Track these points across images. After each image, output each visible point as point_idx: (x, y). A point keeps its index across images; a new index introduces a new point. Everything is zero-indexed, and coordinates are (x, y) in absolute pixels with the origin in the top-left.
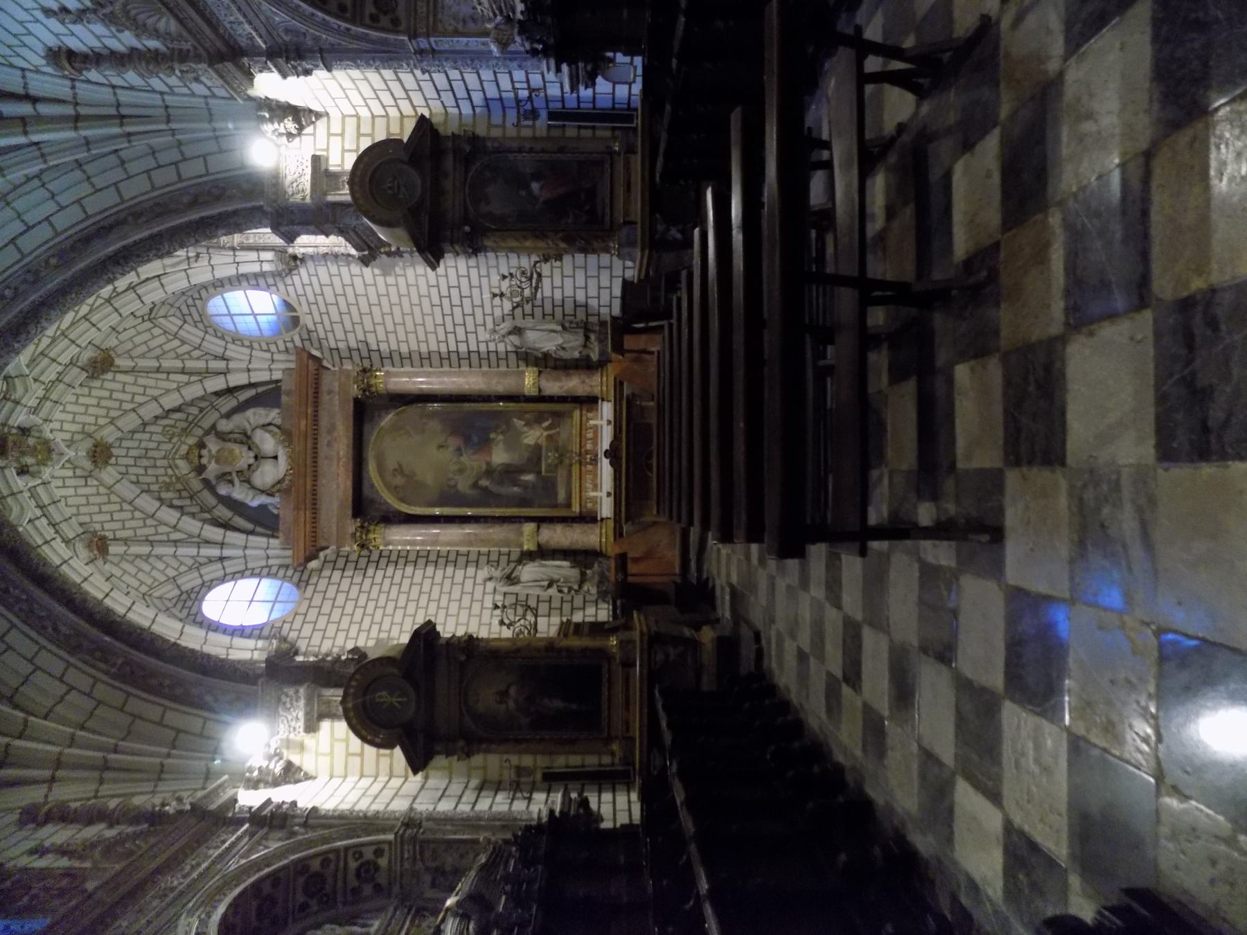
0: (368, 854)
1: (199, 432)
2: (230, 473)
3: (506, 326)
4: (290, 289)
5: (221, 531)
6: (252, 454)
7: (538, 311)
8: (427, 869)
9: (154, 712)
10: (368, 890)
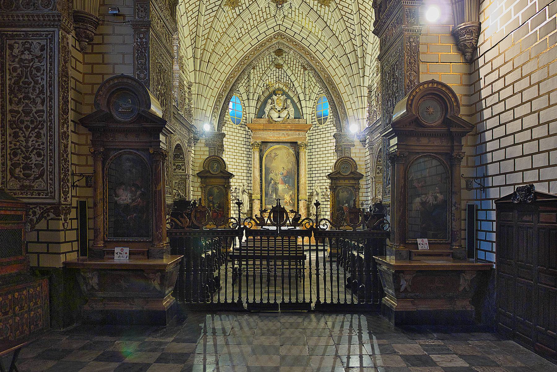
0: (183, 167)
3: (319, 191)
4: (329, 123)
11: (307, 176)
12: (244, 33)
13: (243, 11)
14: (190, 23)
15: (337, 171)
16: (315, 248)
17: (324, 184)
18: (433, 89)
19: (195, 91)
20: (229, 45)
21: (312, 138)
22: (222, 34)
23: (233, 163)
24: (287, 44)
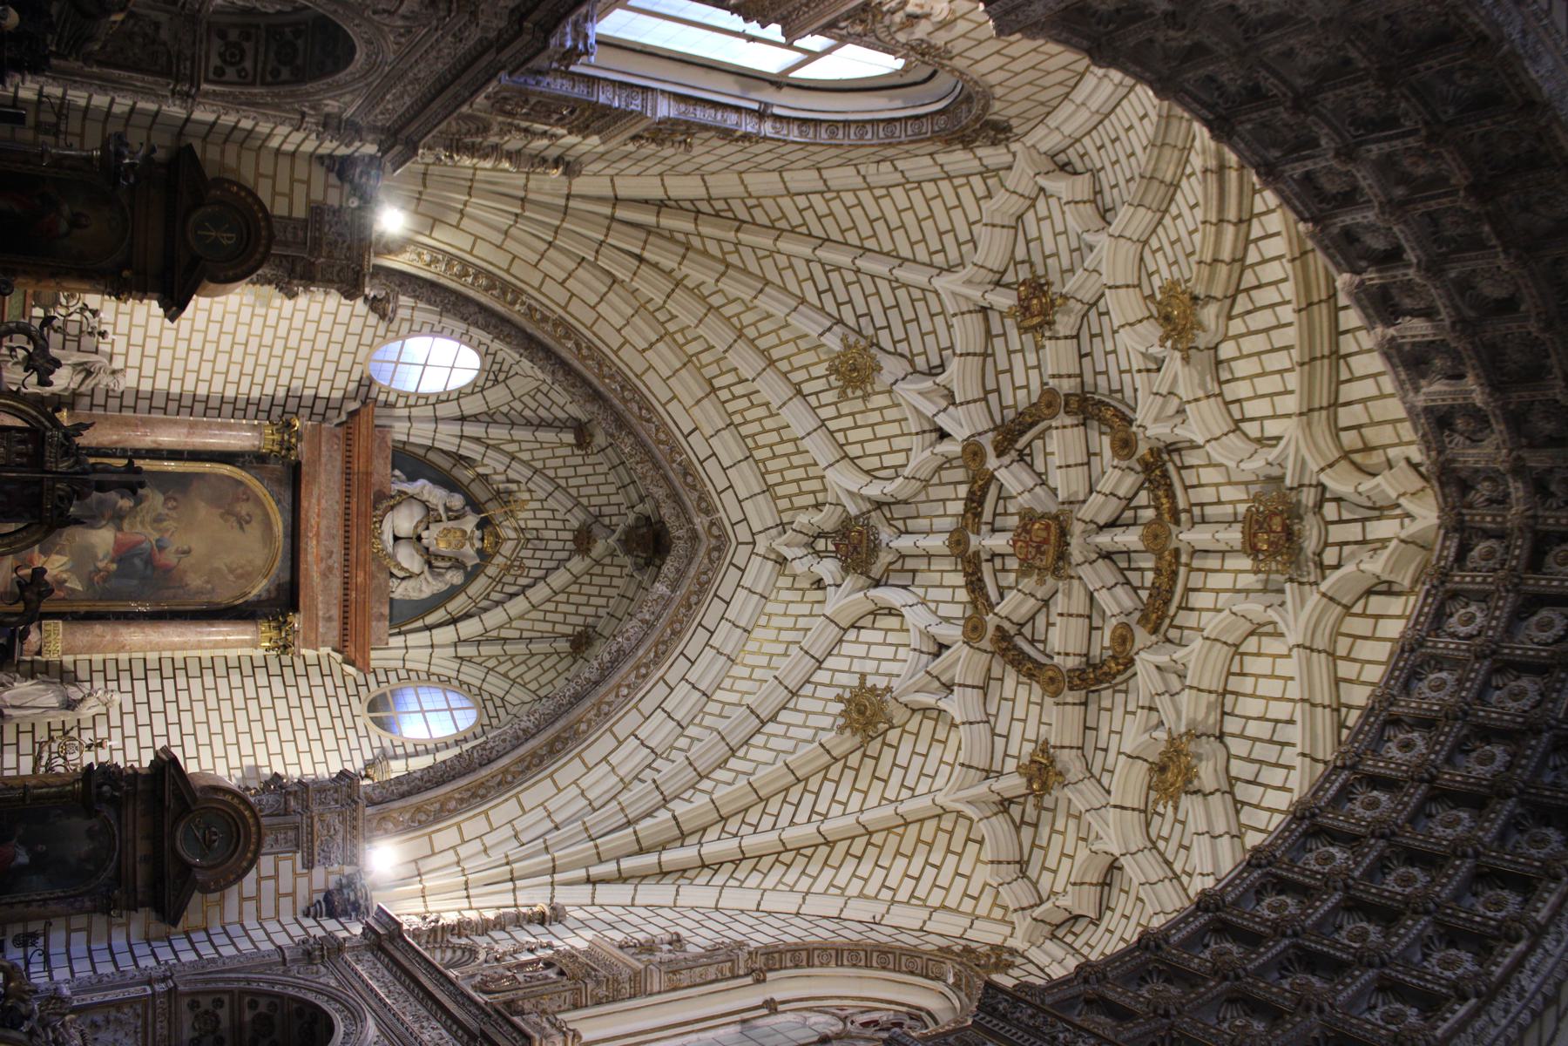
0: (231, 73)
1: (491, 570)
2: (449, 519)
3: (86, 711)
4: (376, 743)
5: (462, 452)
6: (425, 541)
7: (41, 734)
8: (164, 44)
9: (482, 250)
10: (233, 35)
11: (152, 656)
13: (814, 409)
14: (786, 202)
15: (195, 800)
17: (116, 733)
19: (539, 191)
20: (693, 348)
21: (314, 671)
22: (735, 320)
24: (692, 572)
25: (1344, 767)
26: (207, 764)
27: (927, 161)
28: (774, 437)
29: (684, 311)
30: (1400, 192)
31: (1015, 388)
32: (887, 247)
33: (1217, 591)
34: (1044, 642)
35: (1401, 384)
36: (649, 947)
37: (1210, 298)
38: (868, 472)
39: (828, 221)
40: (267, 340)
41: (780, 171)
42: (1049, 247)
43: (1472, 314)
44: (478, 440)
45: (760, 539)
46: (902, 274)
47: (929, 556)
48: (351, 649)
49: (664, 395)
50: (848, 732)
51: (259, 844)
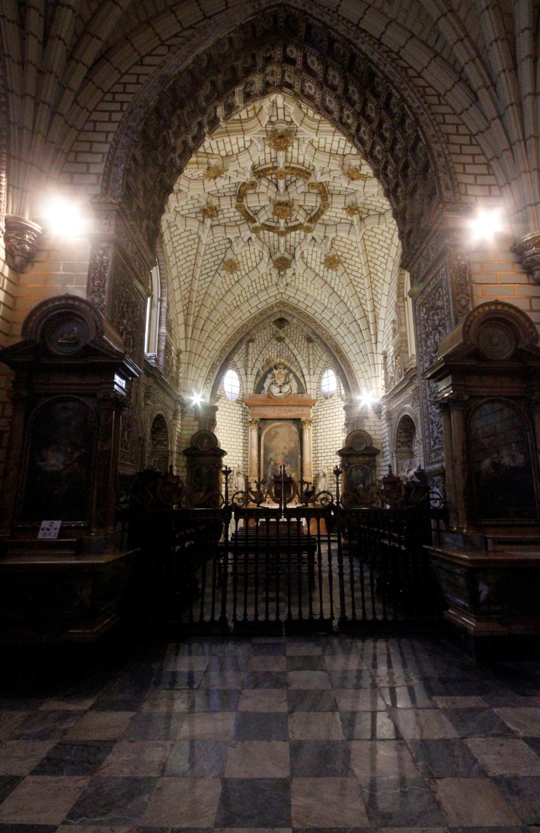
1: (289, 365)
3: (326, 471)
9: (203, 374)
10: (155, 443)
11: (312, 456)
12: (242, 301)
14: (183, 288)
16: (326, 539)
18: (496, 311)
20: (226, 313)
21: (317, 414)
23: (227, 442)
24: (290, 312)
25: (353, 140)
26: (341, 442)
27: (167, 246)
28: (251, 288)
29: (216, 316)
30: (183, 128)
31: (235, 216)
32: (194, 257)
33: (298, 154)
34: (313, 207)
35: (237, 112)
36: (394, 330)
37: (208, 163)
38: (261, 260)
39: (188, 275)
40: (227, 428)
41: (174, 291)
42: (191, 206)
43: (216, 94)
44: (252, 370)
45: (280, 291)
46: (202, 252)
47: (286, 241)
48: (311, 404)
49: (240, 321)
50: (338, 268)
51: (361, 430)
